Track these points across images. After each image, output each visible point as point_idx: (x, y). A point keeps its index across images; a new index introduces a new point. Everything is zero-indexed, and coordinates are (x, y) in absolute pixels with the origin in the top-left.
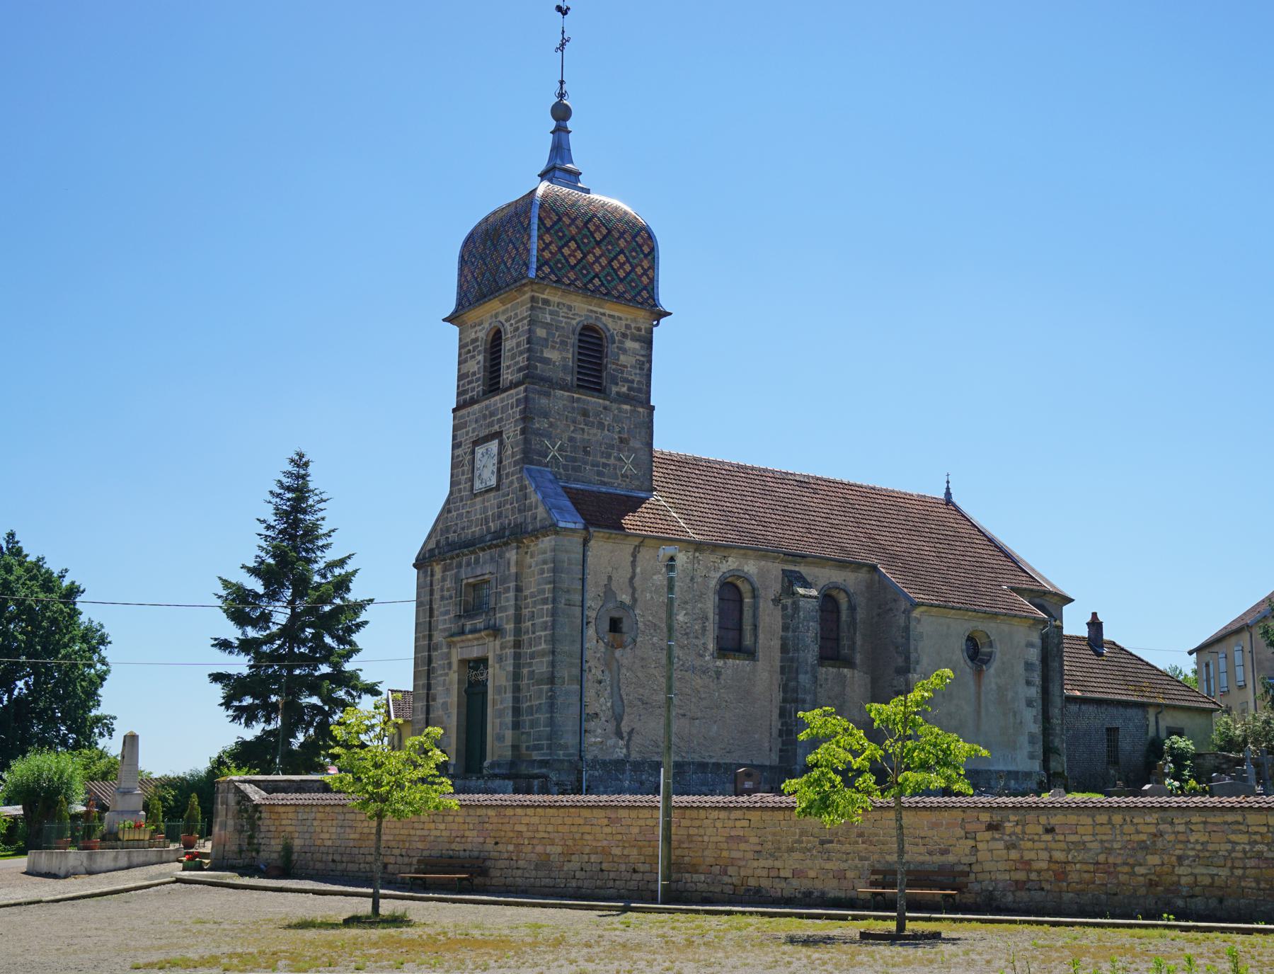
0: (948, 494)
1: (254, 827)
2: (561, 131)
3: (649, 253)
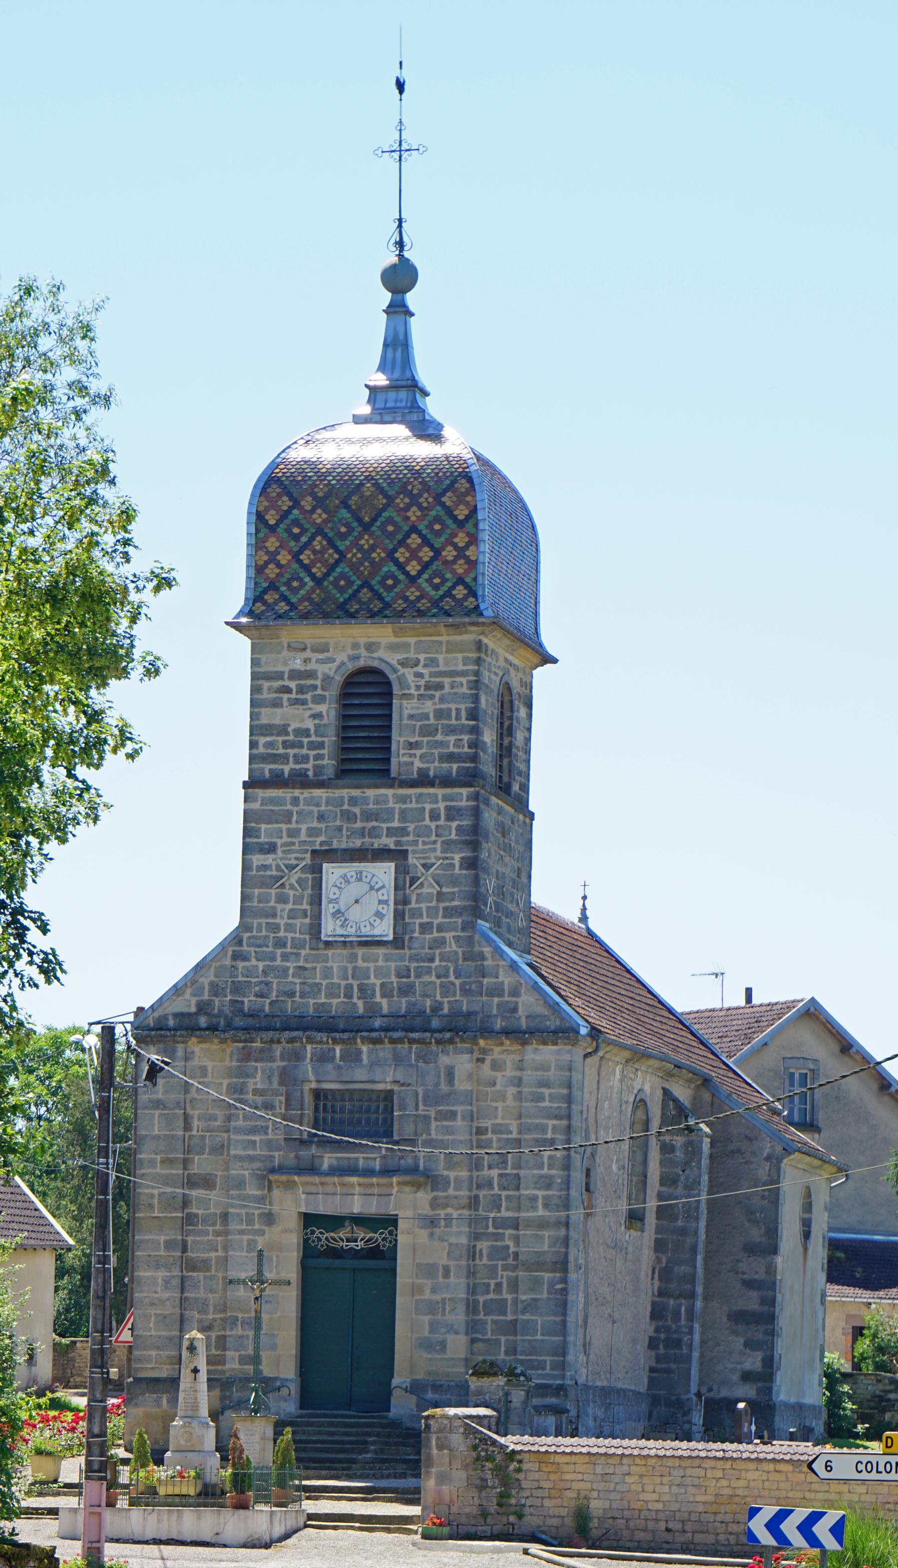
0: (584, 918)
1: (507, 1483)
2: (398, 310)
3: (467, 518)
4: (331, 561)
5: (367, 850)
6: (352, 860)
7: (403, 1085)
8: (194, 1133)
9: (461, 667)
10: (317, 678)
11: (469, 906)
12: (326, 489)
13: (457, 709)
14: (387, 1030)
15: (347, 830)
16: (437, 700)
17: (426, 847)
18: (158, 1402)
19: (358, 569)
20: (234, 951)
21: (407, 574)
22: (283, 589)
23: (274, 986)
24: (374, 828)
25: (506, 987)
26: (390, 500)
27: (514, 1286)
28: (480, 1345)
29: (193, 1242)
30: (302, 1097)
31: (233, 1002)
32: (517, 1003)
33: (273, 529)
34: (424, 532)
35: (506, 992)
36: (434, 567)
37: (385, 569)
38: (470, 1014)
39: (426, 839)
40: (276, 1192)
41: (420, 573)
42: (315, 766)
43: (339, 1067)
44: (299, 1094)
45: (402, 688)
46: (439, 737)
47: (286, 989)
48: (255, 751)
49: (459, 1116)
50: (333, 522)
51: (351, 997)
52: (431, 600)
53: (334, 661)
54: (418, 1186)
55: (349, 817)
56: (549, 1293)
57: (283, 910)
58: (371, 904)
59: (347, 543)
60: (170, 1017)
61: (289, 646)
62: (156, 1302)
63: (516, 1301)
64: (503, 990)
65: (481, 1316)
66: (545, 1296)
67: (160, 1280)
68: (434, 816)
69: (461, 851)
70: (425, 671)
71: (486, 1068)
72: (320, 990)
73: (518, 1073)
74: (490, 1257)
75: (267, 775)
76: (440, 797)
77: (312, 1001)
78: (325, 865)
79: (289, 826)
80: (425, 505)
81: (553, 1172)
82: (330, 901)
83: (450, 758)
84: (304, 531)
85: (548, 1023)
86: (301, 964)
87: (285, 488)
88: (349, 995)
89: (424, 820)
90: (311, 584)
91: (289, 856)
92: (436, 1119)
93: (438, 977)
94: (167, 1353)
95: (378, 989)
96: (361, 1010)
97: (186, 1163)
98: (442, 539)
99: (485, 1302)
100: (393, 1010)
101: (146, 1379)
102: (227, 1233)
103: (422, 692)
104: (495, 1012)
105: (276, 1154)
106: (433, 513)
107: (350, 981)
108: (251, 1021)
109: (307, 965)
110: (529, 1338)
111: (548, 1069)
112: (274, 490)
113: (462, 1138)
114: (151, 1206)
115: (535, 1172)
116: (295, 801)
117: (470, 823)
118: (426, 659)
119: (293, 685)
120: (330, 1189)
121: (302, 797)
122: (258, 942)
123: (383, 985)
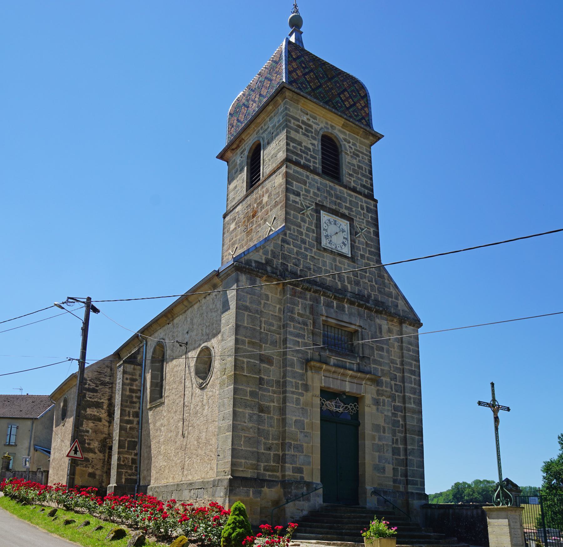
6: (333, 214)
58: (341, 236)
60: (253, 262)
62: (245, 428)
67: (247, 415)
68: (362, 208)
83: (364, 186)
93: (369, 281)
96: (340, 287)
109: (315, 257)
116: (307, 177)
121: (310, 177)
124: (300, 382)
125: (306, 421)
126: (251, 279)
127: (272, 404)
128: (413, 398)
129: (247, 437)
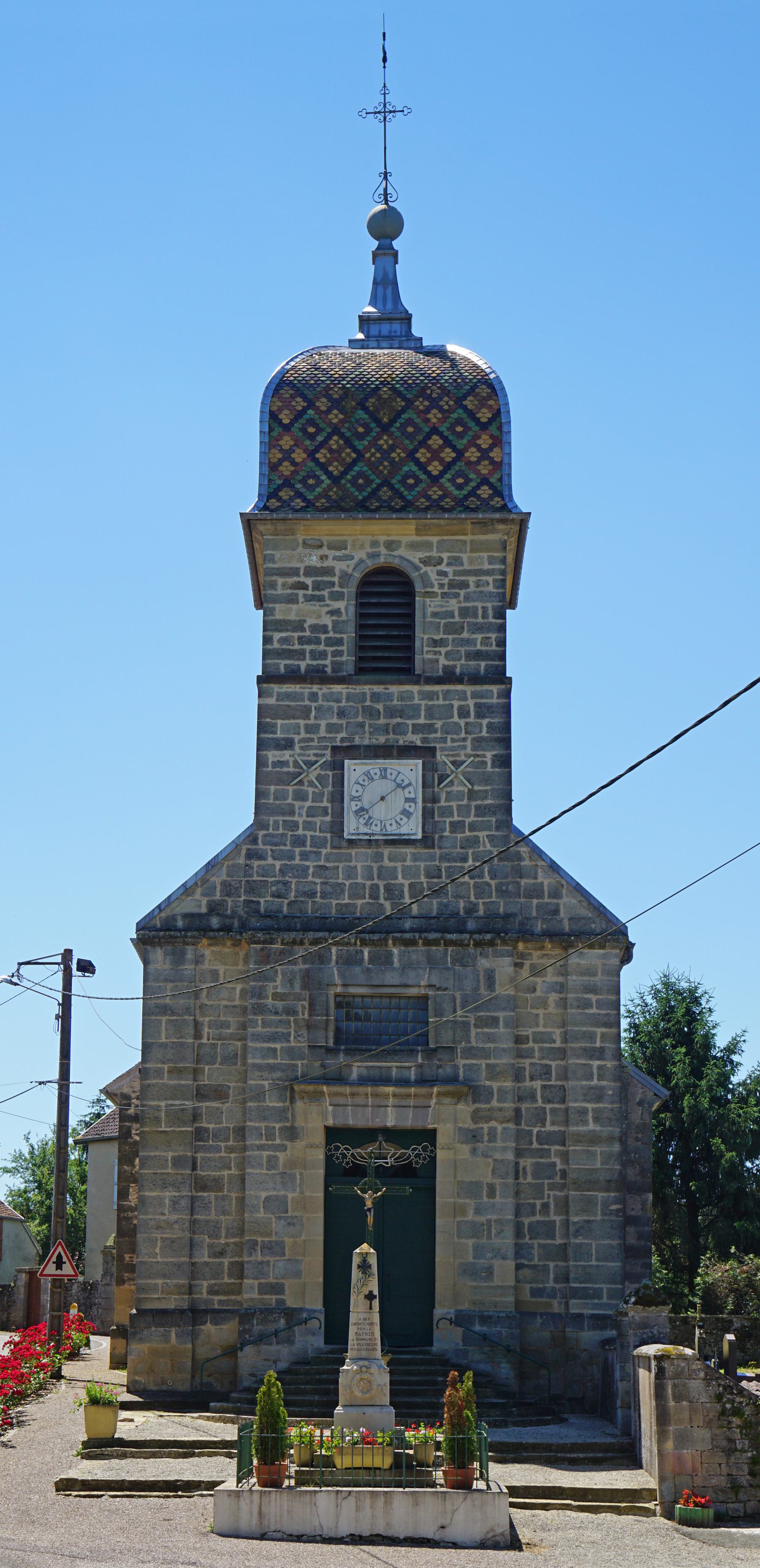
2: (385, 255)
3: (491, 421)
4: (349, 460)
5: (393, 746)
6: (376, 757)
7: (439, 989)
8: (205, 1041)
9: (486, 566)
10: (334, 575)
11: (502, 804)
12: (341, 392)
13: (483, 607)
14: (420, 930)
15: (370, 726)
16: (462, 598)
17: (456, 744)
18: (166, 1338)
19: (377, 468)
20: (248, 850)
21: (428, 474)
22: (299, 486)
23: (293, 886)
24: (399, 724)
25: (546, 888)
26: (409, 403)
27: (564, 1206)
28: (526, 1272)
29: (203, 1159)
30: (327, 1002)
31: (247, 903)
32: (558, 905)
33: (287, 428)
34: (446, 434)
35: (546, 893)
36: (457, 468)
37: (406, 469)
38: (507, 916)
39: (455, 736)
40: (299, 1105)
41: (442, 474)
42: (332, 662)
43: (368, 970)
44: (324, 999)
45: (425, 587)
46: (465, 635)
47: (306, 889)
48: (269, 647)
49: (501, 1022)
50: (350, 422)
51: (377, 898)
52: (454, 499)
53: (352, 558)
54: (459, 1097)
55: (372, 713)
56: (604, 1214)
57: (301, 808)
58: (397, 801)
59: (366, 443)
60: (179, 918)
61: (304, 543)
62: (163, 1224)
63: (566, 1224)
64: (543, 891)
65: (527, 1240)
66: (599, 1218)
67: (167, 1201)
68: (463, 713)
69: (493, 748)
70: (449, 570)
71: (525, 972)
72: (343, 891)
73: (560, 979)
74: (535, 1175)
75: (282, 670)
76: (469, 694)
77: (334, 902)
78: (346, 762)
79: (307, 722)
80: (446, 407)
81: (604, 1083)
82: (353, 799)
83: (478, 655)
84: (319, 430)
85: (593, 926)
86: (322, 863)
87: (298, 390)
88: (374, 895)
89: (452, 717)
90: (328, 482)
91: (307, 752)
92: (476, 1026)
94: (175, 1281)
95: (406, 890)
97: (196, 1073)
98: (465, 441)
99: (530, 1224)
100: (424, 912)
101: (151, 1310)
102: (244, 1149)
103: (446, 590)
104: (534, 914)
105: (299, 1063)
106: (455, 415)
107: (376, 881)
108: (269, 922)
109: (328, 865)
110: (582, 1263)
111: (595, 974)
112: (286, 392)
113: (505, 1046)
114: (157, 1120)
115: (584, 1083)
116: (314, 697)
117: (502, 720)
118: (449, 558)
119: (309, 581)
120: (360, 1100)
121: (320, 693)
122: (275, 840)
123: (411, 886)
124: (277, 1126)
125: (290, 1196)
126: (174, 953)
127: (226, 1173)
128: (593, 1109)
129: (167, 1238)
